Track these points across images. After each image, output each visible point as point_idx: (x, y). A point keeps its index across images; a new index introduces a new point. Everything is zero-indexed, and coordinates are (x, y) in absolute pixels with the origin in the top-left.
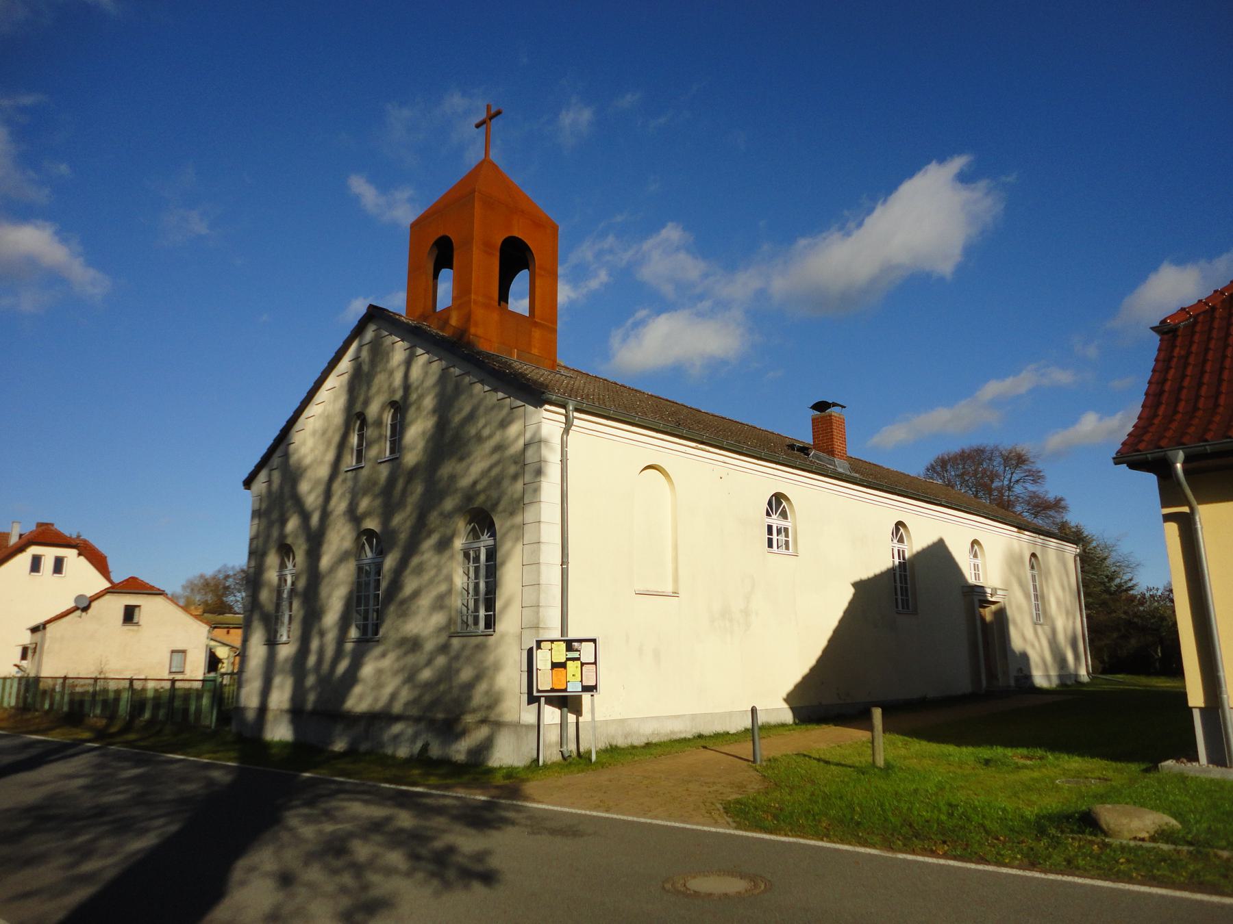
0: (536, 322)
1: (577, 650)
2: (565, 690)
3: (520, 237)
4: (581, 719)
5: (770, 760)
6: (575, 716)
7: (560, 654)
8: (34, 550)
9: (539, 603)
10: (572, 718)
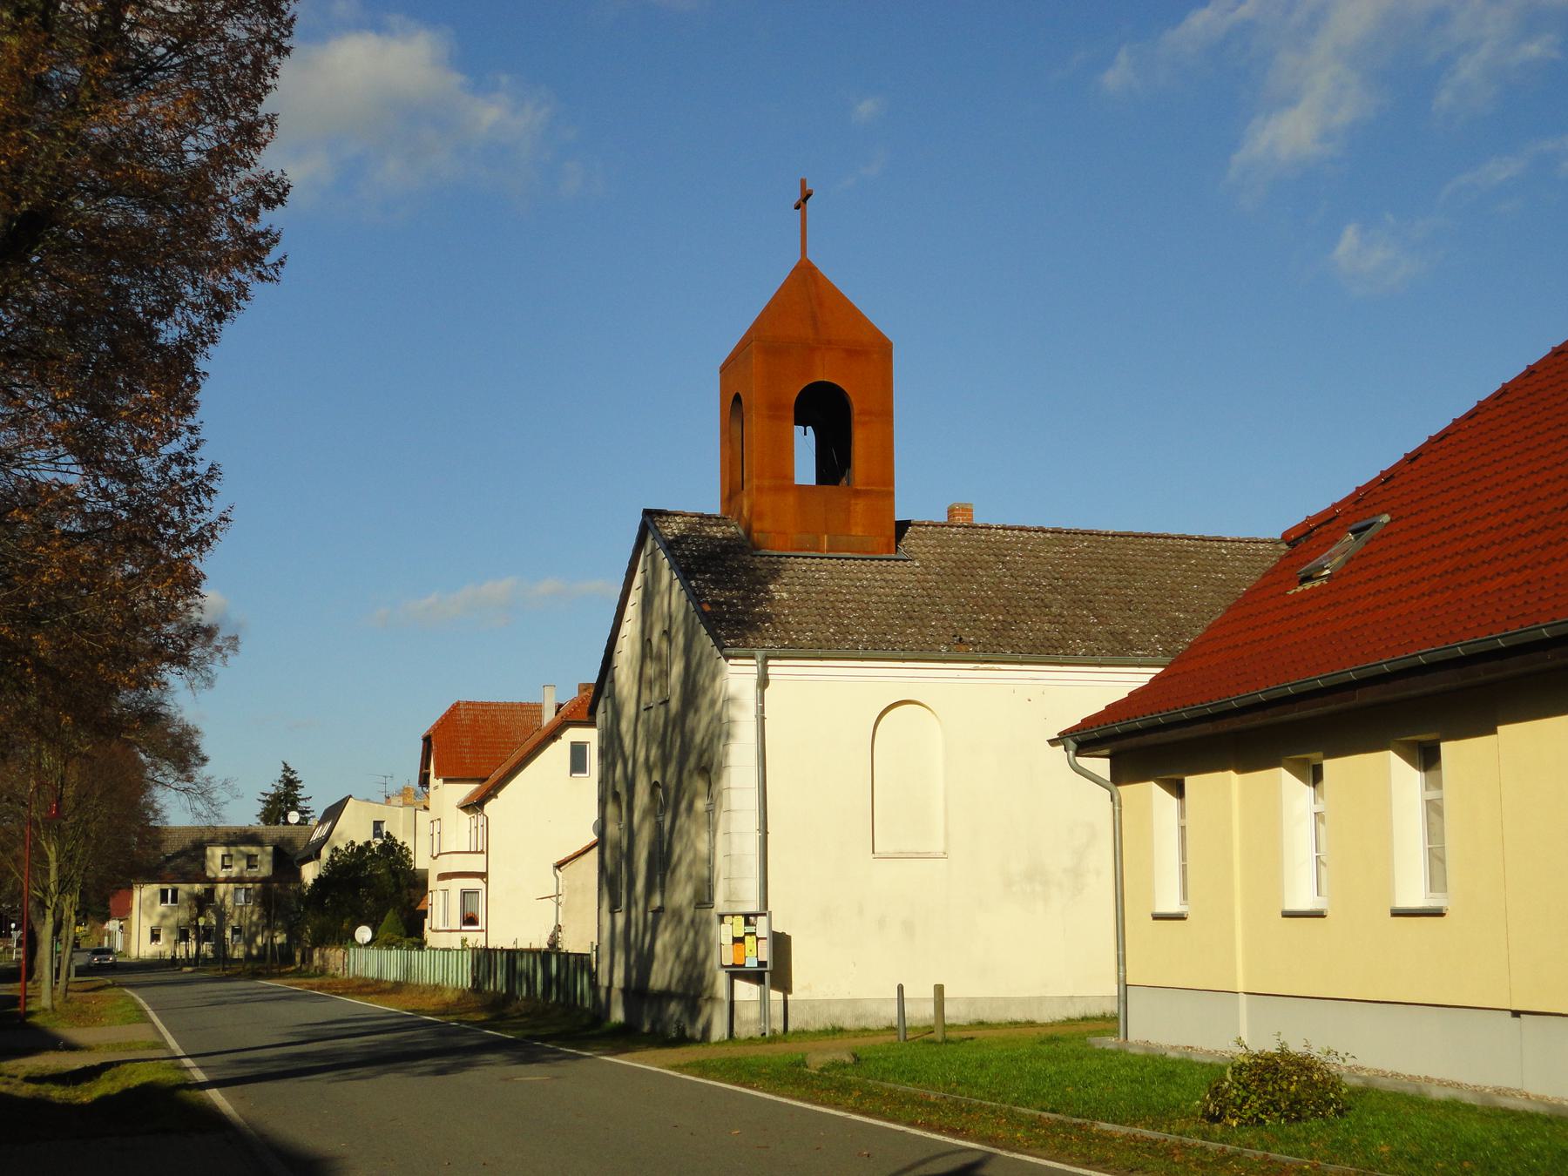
1: (753, 925)
2: (743, 966)
4: (789, 997)
5: (1378, 1071)
6: (781, 994)
7: (739, 928)
8: (573, 734)
9: (730, 873)
10: (776, 996)
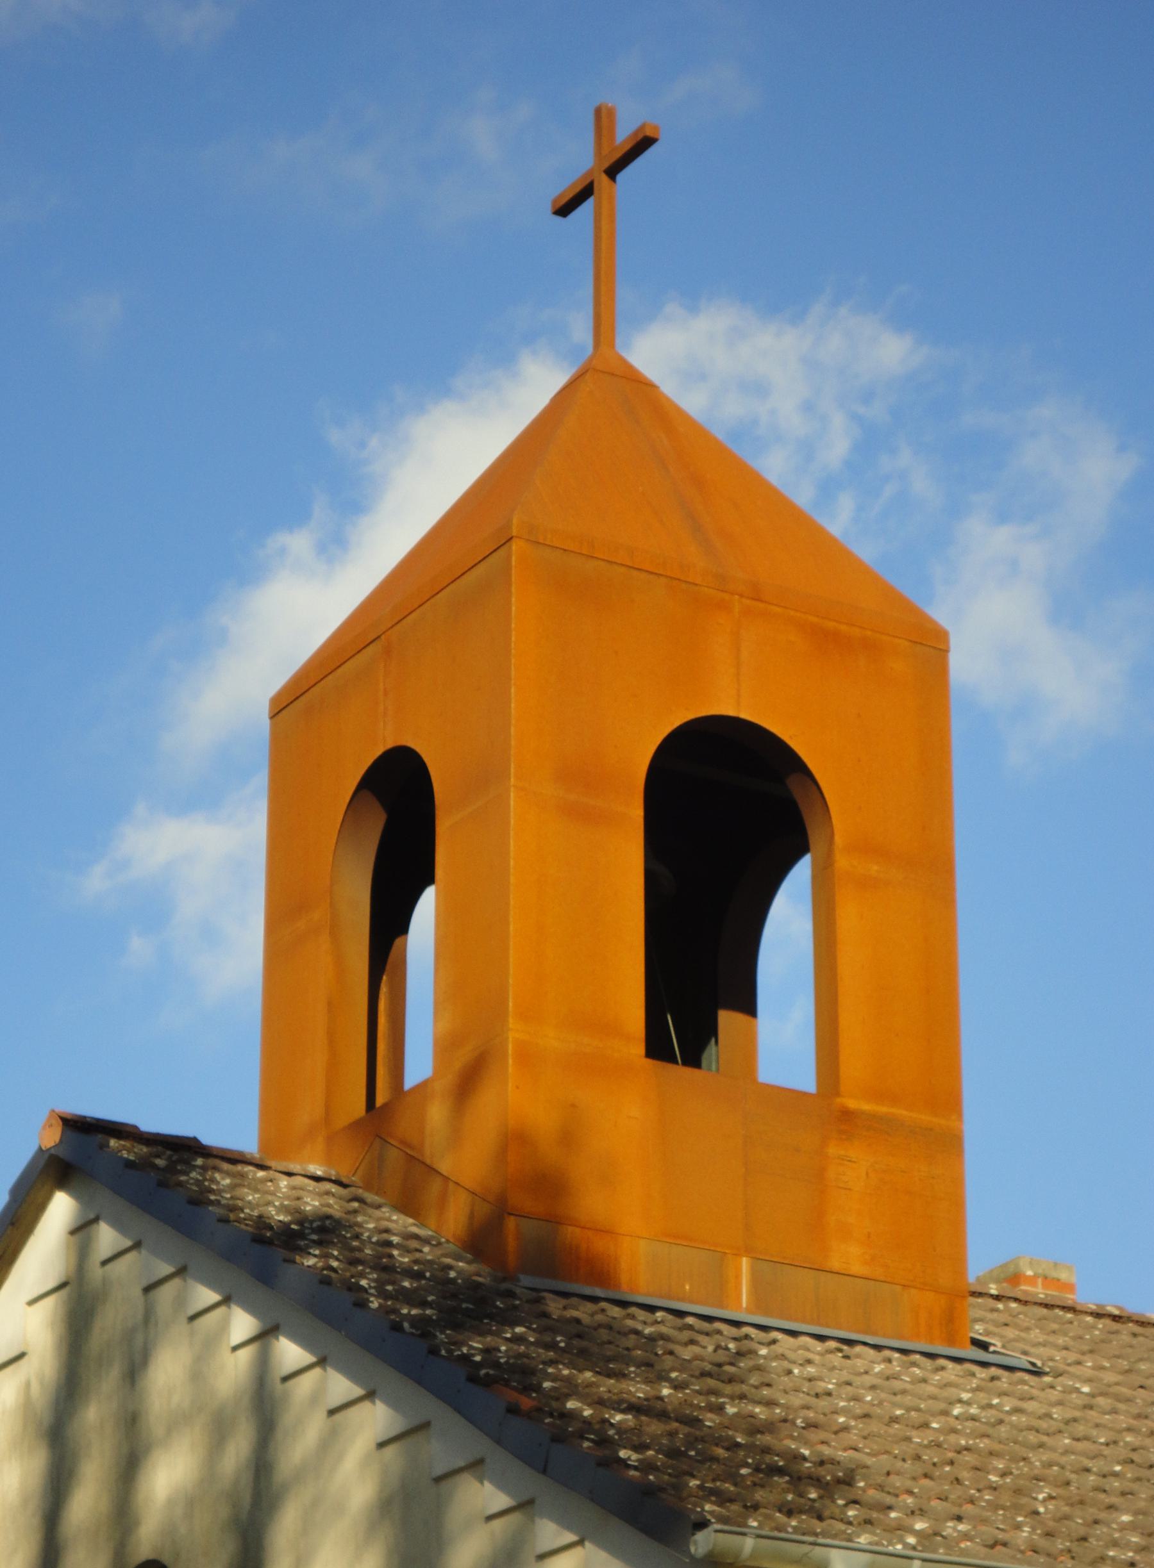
0: (847, 1115)
3: (744, 715)
